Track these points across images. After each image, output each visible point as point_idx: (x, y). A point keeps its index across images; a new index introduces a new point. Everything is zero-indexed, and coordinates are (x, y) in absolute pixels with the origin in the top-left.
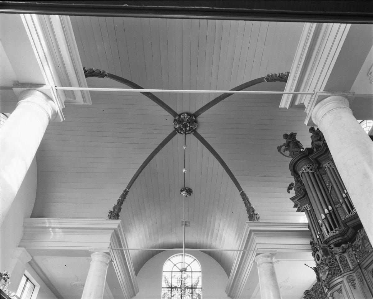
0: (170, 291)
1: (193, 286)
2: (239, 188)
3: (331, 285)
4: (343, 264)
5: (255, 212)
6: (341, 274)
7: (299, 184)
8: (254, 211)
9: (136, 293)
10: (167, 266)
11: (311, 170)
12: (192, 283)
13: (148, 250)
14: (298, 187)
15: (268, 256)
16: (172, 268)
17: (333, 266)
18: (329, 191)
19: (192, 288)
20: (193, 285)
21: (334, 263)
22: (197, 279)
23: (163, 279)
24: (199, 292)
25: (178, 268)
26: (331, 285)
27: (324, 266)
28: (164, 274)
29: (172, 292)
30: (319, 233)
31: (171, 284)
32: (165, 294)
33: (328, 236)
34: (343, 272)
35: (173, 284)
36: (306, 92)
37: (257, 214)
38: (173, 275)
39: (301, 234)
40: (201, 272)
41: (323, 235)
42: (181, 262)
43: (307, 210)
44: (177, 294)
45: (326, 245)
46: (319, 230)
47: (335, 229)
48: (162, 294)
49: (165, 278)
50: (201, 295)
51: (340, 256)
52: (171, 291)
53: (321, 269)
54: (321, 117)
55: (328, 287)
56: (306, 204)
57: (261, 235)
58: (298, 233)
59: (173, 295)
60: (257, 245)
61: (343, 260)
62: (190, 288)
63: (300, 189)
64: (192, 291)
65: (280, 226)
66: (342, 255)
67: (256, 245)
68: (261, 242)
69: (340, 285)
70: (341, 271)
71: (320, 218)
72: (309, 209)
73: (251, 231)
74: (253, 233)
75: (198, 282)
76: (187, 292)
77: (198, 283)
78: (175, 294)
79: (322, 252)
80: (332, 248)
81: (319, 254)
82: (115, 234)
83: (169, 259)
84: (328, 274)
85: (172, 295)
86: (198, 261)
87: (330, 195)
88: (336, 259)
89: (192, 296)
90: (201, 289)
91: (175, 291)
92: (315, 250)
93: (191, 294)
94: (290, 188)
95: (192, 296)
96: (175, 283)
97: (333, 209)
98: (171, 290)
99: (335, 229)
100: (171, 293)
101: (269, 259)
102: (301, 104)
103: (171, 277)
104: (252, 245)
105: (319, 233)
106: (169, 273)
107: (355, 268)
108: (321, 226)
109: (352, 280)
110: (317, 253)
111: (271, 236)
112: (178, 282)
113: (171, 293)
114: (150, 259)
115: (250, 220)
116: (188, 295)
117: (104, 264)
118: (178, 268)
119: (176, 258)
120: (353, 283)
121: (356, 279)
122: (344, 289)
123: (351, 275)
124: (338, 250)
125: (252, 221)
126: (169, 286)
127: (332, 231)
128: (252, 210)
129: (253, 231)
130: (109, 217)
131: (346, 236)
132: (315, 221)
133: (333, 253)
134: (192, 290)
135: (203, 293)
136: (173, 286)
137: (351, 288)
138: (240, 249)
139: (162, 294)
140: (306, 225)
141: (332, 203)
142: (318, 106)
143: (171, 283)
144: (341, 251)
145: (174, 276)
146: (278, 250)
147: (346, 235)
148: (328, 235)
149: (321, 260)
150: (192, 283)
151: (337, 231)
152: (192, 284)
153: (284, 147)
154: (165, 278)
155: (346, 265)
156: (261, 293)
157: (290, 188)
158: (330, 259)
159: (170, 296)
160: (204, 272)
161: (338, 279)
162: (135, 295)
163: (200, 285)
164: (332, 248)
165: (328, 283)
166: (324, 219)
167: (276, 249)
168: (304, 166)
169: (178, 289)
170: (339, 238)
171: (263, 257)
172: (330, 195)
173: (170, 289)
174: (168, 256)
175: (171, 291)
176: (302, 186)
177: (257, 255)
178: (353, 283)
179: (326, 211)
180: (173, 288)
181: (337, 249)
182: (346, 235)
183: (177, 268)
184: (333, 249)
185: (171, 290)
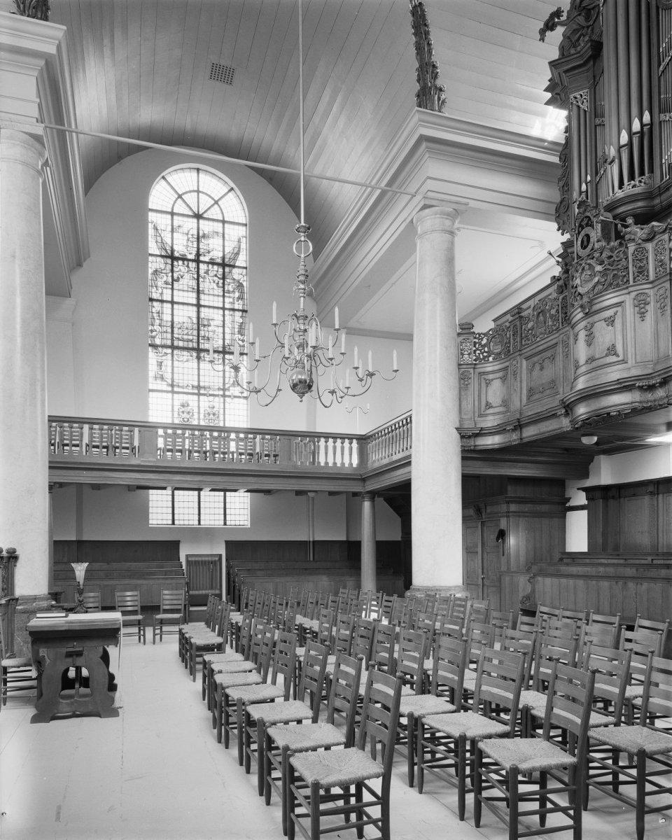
0: (170, 266)
1: (226, 260)
3: (596, 307)
4: (638, 265)
5: (439, 82)
6: (627, 288)
7: (581, 20)
8: (435, 76)
9: (83, 260)
10: (160, 195)
12: (224, 251)
13: (110, 141)
14: (575, 27)
15: (448, 215)
16: (173, 205)
19: (223, 265)
20: (227, 257)
21: (618, 261)
22: (236, 243)
23: (151, 231)
24: (241, 276)
25: (188, 206)
26: (596, 307)
27: (594, 265)
28: (152, 216)
29: (175, 269)
30: (589, 178)
31: (172, 247)
32: (156, 271)
33: (620, 194)
34: (631, 283)
35: (175, 247)
37: (441, 90)
38: (176, 224)
39: (530, 168)
40: (246, 225)
41: (597, 185)
42: (194, 191)
43: (579, 106)
44: (187, 276)
45: (609, 215)
46: (591, 171)
47: (640, 179)
48: (150, 271)
49: (156, 229)
50: (245, 284)
51: (636, 247)
52: (172, 266)
53: (583, 269)
55: (587, 310)
56: (582, 89)
57: (441, 154)
58: (524, 164)
59: (178, 277)
60: (428, 180)
61: (641, 255)
62: (218, 264)
63: (578, 35)
64: (224, 272)
65: (428, 122)
66: (643, 246)
67: (425, 180)
68: (441, 175)
69: (614, 310)
70: (628, 281)
71: (615, 140)
72: (584, 107)
73: (423, 139)
74: (424, 145)
75: (239, 251)
76: (211, 274)
77: (238, 254)
78: (182, 274)
79: (599, 231)
82: (46, 76)
83: (163, 178)
85: (175, 275)
86: (239, 193)
87: (659, 78)
88: (625, 253)
89: (224, 284)
90: (245, 270)
91: (182, 268)
92: (584, 223)
93: (221, 281)
94: (550, 24)
95: (224, 284)
96: (182, 246)
97: (651, 124)
98: (172, 262)
99: (640, 179)
100: (172, 271)
101: (448, 223)
103: (169, 228)
104: (409, 180)
105: (589, 178)
106: (164, 216)
107: (658, 279)
108: (610, 164)
109: (643, 302)
110: (587, 230)
111: (483, 166)
112: (190, 244)
113: (172, 271)
114: (120, 162)
115: (420, 102)
116: (214, 282)
117: (32, 172)
118: (188, 206)
119: (181, 175)
120: (643, 310)
121: (652, 304)
122: (620, 319)
123: (644, 291)
124: (639, 232)
125: (426, 108)
126: (166, 251)
127: (633, 182)
128: (433, 72)
130: (19, 7)
131: (657, 201)
132: (588, 144)
133: (627, 237)
134: (224, 269)
135: (251, 281)
136: (176, 254)
137: (636, 318)
138: (372, 184)
139: (150, 271)
140: (556, 148)
141: (656, 104)
143: (172, 244)
144: (644, 236)
145: (179, 226)
146: (472, 204)
147: (659, 198)
148: (620, 191)
149: (592, 249)
150: (224, 251)
151: (642, 184)
152: (224, 255)
154: (156, 229)
155: (642, 271)
156: (416, 302)
157: (550, 26)
158: (612, 250)
159: (170, 280)
160: (256, 226)
161: (611, 298)
162: (80, 265)
163: (242, 260)
165: (591, 303)
167: (468, 201)
169: (190, 263)
170: (640, 204)
171: (436, 214)
172: (659, 78)
173: (169, 261)
174: (159, 167)
175: (172, 266)
176: (588, 27)
177: (425, 207)
178: (643, 310)
179: (636, 126)
180: (177, 259)
181: (638, 230)
182: (659, 198)
183: (184, 205)
184: (629, 229)
185: (172, 262)
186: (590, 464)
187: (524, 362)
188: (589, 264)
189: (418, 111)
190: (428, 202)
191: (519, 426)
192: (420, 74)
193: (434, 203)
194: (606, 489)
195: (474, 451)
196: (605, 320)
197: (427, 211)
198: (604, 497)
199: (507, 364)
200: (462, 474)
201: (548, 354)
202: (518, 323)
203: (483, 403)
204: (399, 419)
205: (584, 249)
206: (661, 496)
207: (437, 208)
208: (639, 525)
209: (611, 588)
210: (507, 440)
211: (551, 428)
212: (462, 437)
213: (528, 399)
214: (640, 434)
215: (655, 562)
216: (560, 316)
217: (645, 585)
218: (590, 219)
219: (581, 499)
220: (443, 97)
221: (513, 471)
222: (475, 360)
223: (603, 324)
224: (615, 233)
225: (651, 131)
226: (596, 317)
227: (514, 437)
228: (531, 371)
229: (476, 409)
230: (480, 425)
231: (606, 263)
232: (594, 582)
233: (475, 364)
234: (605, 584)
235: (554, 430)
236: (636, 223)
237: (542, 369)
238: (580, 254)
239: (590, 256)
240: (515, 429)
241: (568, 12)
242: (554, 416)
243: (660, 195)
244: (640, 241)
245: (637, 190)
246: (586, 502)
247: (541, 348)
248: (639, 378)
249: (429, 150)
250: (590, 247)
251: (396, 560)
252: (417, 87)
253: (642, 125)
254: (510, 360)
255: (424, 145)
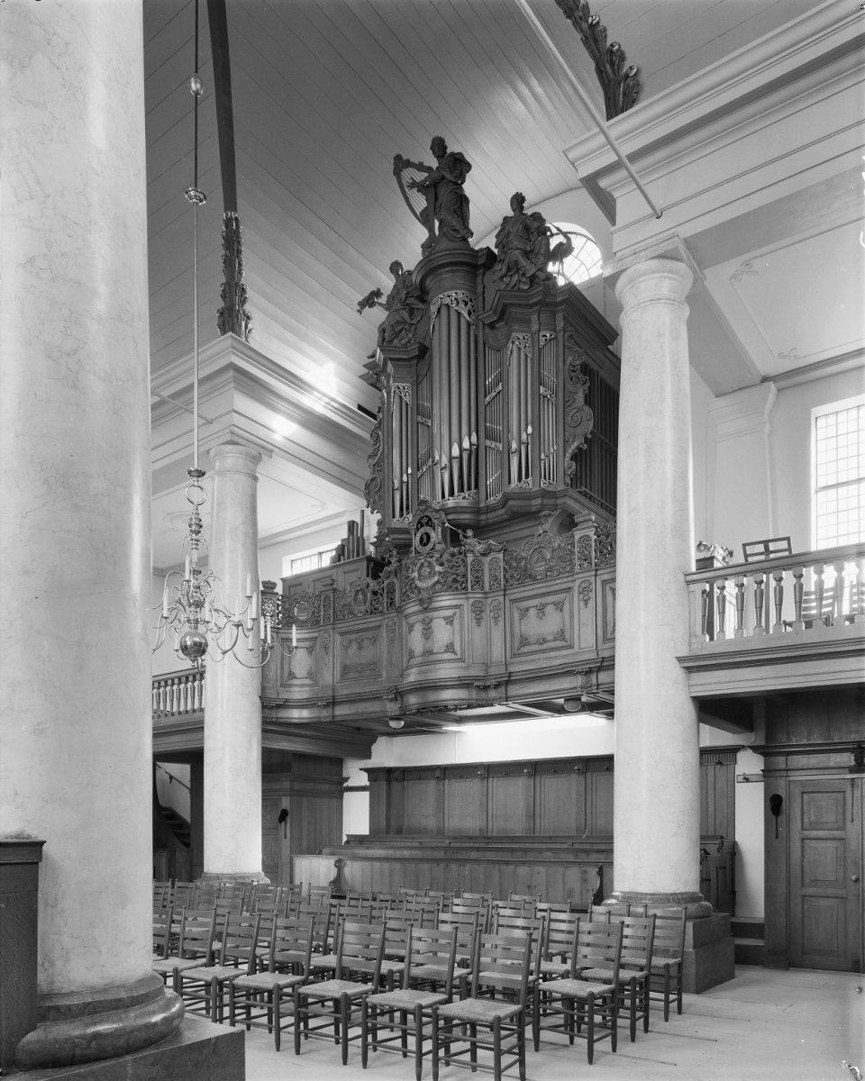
2: (230, 203)
8: (244, 301)
11: (469, 314)
17: (453, 571)
18: (488, 399)
30: (410, 471)
36: (642, 182)
37: (248, 318)
54: (649, 299)
56: (405, 382)
61: (478, 569)
67: (229, 412)
73: (232, 366)
74: (231, 373)
80: (466, 537)
81: (433, 535)
84: (438, 582)
102: (611, 196)
105: (410, 471)
128: (242, 295)
129: (234, 369)
131: (483, 517)
142: (655, 263)
148: (451, 498)
153: (420, 176)
155: (478, 581)
157: (369, 301)
161: (446, 600)
164: (466, 537)
165: (430, 599)
166: (454, 458)
167: (274, 448)
168: (459, 289)
179: (466, 444)
184: (468, 541)
186: (372, 744)
187: (338, 638)
188: (429, 562)
189: (232, 337)
190: (235, 439)
191: (333, 703)
192: (227, 290)
193: (240, 440)
194: (389, 772)
195: (275, 724)
196: (445, 618)
197: (231, 447)
198: (385, 779)
199: (315, 635)
200: (263, 748)
201: (369, 634)
202: (331, 595)
203: (286, 674)
204: (166, 677)
205: (425, 545)
206: (447, 781)
207: (242, 447)
208: (422, 807)
209: (431, 870)
210: (314, 715)
211: (370, 709)
212: (264, 707)
213: (342, 676)
214: (440, 723)
215: (452, 845)
216: (385, 600)
217: (468, 866)
218: (430, 519)
219: (363, 780)
220: (250, 326)
221: (281, 744)
222: (278, 624)
223: (443, 622)
224: (454, 538)
225: (477, 450)
226: (435, 614)
227: (325, 714)
228: (346, 648)
229: (279, 677)
230: (285, 696)
231: (446, 565)
232: (413, 865)
233: (278, 628)
234: (426, 866)
235: (374, 713)
236: (474, 536)
237: (360, 648)
238: (419, 549)
239: (430, 555)
240: (326, 706)
241: (389, 297)
242: (378, 698)
243: (487, 513)
244: (478, 555)
245: (465, 503)
246: (368, 784)
247: (360, 627)
248: (477, 678)
249: (236, 380)
250: (430, 545)
251: (596, 848)
252: (221, 304)
253: (471, 444)
254: (319, 631)
255: (231, 373)
